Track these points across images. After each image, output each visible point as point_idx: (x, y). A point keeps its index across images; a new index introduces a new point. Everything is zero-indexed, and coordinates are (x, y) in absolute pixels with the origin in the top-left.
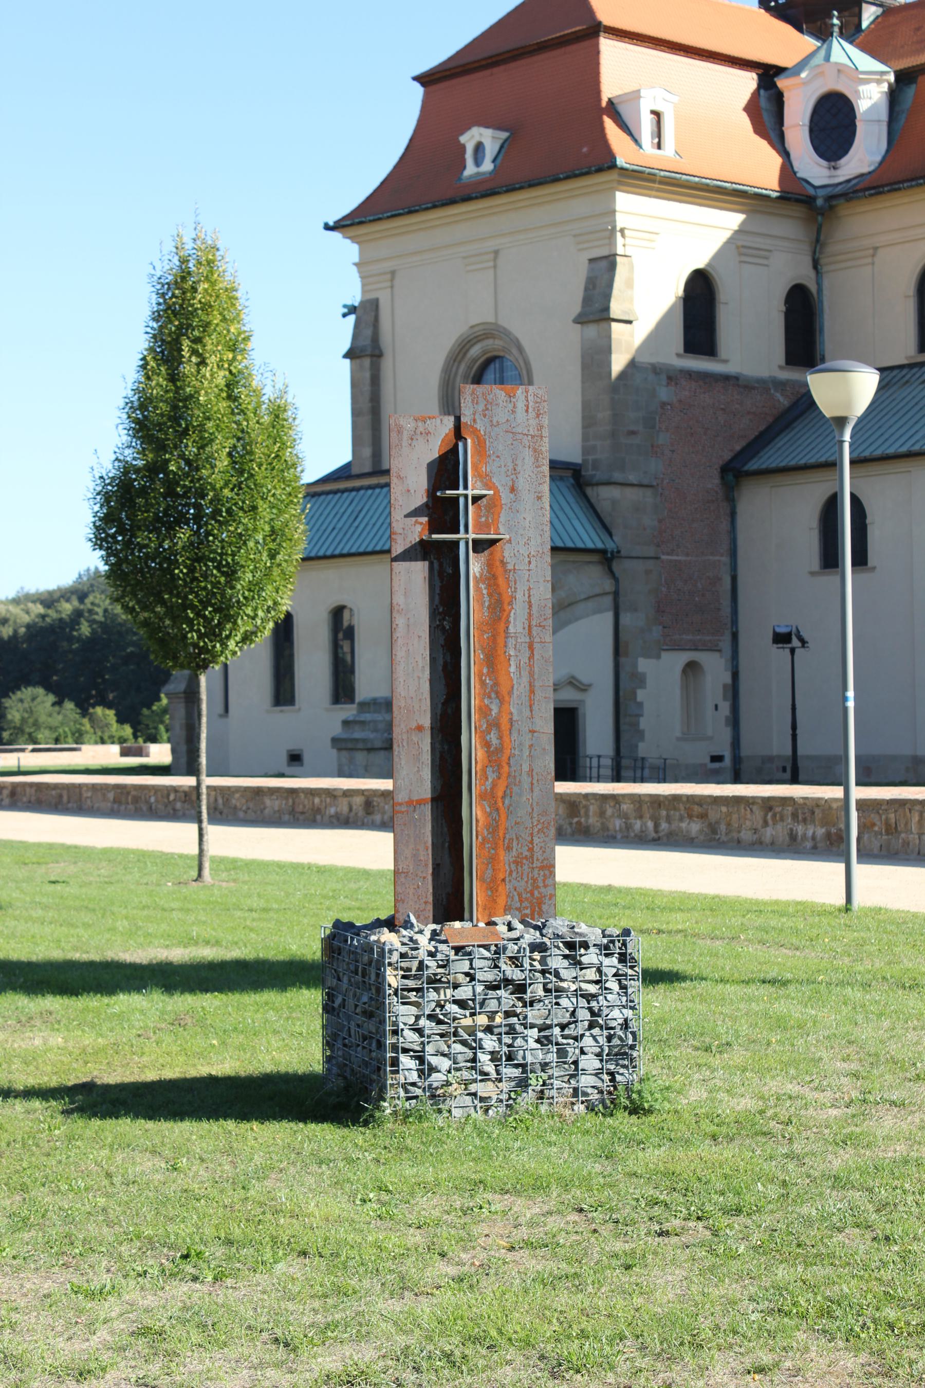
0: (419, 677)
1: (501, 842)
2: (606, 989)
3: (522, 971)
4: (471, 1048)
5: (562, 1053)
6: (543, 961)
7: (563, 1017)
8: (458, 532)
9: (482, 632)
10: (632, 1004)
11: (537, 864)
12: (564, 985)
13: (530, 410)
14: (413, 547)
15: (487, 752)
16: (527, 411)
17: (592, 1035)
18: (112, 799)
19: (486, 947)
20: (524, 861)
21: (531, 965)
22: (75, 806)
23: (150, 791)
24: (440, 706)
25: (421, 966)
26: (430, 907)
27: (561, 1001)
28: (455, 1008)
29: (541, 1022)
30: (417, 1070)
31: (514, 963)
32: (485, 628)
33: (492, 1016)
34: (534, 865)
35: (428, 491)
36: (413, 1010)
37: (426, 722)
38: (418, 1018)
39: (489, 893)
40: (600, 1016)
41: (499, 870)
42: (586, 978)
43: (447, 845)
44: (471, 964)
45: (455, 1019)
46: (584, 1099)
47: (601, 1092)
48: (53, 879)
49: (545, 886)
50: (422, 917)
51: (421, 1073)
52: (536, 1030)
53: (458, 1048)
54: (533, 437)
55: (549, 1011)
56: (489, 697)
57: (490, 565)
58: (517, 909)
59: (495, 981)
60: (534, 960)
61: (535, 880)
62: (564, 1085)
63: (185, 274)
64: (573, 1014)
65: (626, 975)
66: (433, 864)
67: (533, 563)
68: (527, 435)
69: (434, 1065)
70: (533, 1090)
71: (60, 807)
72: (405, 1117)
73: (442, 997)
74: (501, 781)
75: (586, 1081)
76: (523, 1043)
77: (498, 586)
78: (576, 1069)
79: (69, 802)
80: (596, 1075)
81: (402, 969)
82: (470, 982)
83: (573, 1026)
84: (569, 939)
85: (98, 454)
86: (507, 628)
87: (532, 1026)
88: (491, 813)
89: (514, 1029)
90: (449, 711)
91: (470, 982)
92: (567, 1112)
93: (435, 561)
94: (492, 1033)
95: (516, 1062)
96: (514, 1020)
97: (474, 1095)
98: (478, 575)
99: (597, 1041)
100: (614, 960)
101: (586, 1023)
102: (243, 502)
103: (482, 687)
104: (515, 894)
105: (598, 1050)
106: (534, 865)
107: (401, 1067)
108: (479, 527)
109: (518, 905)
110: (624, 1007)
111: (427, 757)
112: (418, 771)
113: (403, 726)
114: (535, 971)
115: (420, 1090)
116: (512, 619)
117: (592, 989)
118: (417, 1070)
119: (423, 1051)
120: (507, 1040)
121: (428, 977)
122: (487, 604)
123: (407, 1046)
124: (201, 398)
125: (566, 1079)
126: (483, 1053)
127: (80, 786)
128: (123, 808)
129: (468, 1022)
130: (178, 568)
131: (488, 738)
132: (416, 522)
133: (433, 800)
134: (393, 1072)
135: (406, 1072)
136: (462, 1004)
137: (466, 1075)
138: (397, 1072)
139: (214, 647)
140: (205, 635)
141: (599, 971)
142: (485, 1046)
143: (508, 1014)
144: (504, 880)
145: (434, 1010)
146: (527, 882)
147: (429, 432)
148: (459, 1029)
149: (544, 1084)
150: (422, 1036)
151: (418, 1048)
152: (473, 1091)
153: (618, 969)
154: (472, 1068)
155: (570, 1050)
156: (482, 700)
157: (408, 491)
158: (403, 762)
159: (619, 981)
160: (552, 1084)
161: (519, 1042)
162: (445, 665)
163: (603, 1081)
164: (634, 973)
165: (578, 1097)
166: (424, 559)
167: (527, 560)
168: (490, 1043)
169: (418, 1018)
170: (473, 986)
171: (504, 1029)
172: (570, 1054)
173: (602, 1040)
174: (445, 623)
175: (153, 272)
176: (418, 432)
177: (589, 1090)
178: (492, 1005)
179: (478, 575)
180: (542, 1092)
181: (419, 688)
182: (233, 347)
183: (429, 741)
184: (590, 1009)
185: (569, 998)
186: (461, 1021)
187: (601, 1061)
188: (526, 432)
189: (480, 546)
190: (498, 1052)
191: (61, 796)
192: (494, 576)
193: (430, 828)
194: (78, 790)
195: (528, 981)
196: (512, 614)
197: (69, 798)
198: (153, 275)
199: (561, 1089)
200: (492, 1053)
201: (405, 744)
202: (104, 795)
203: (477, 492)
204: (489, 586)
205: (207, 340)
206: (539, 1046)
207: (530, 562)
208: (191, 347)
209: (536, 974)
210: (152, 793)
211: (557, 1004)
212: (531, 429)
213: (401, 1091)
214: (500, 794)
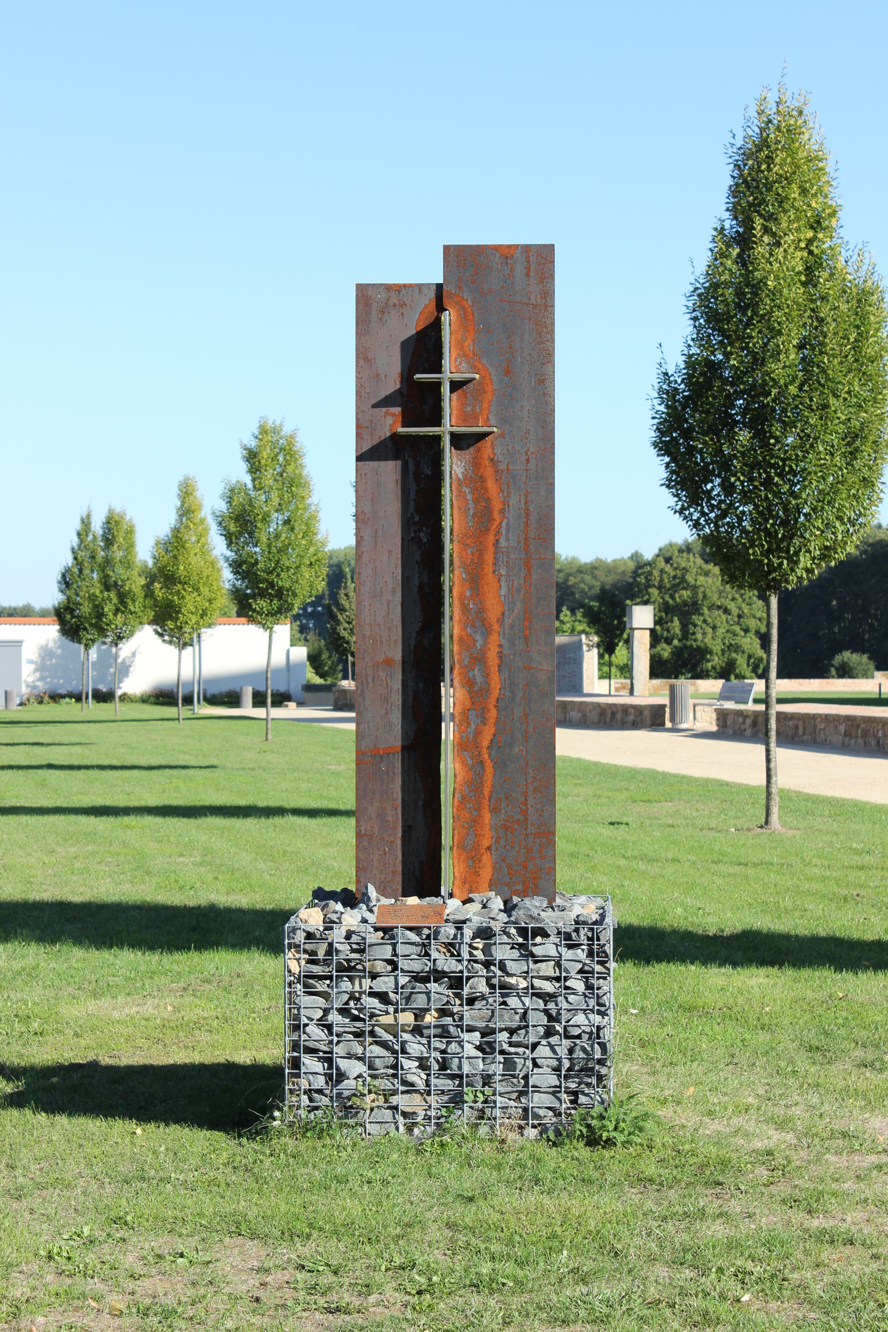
0: (388, 602)
1: (486, 802)
2: (567, 988)
3: (459, 961)
4: (395, 1052)
5: (509, 1064)
6: (486, 950)
7: (512, 1020)
8: (439, 424)
9: (464, 546)
10: (603, 1009)
11: (532, 830)
12: (512, 980)
13: (532, 273)
14: (383, 444)
15: (469, 692)
16: (528, 275)
17: (549, 1044)
18: (843, 732)
19: (416, 930)
20: (516, 826)
21: (471, 954)
22: (810, 738)
23: (878, 724)
24: (414, 635)
25: (330, 950)
26: (399, 878)
27: (509, 1000)
28: (374, 1002)
29: (484, 1024)
30: (325, 1074)
31: (449, 951)
32: (468, 542)
33: (419, 1014)
34: (529, 831)
35: (402, 374)
36: (320, 1001)
37: (397, 655)
38: (326, 1012)
39: (471, 863)
40: (559, 1021)
41: (484, 835)
42: (541, 974)
43: (421, 803)
44: (394, 950)
45: (372, 1016)
46: (536, 1122)
47: (558, 1114)
48: (613, 820)
49: (542, 857)
50: (389, 890)
51: (329, 1077)
52: (477, 1034)
53: (377, 1050)
54: (535, 306)
55: (493, 1011)
56: (473, 626)
57: (476, 464)
58: (505, 884)
59: (422, 972)
60: (476, 949)
61: (529, 850)
62: (512, 1103)
63: (763, 143)
64: (524, 1016)
65: (592, 972)
66: (403, 826)
67: (533, 463)
68: (528, 304)
69: (343, 1069)
70: (471, 1107)
71: (796, 739)
72: (305, 1129)
73: (357, 988)
74: (486, 728)
75: (539, 1101)
76: (459, 1050)
77: (486, 489)
78: (526, 1085)
79: (804, 734)
80: (554, 1093)
81: (305, 951)
82: (393, 971)
83: (523, 1031)
84: (523, 925)
85: (663, 349)
86: (497, 541)
87: (471, 1029)
88: (473, 766)
89: (449, 1032)
90: (426, 642)
91: (393, 971)
92: (512, 1136)
93: (410, 460)
94: (422, 1036)
95: (449, 1071)
96: (448, 1020)
97: (395, 1108)
98: (460, 476)
99: (554, 1051)
100: (581, 954)
101: (541, 1031)
102: (811, 400)
103: (463, 613)
104: (504, 865)
105: (555, 1063)
106: (529, 831)
107: (303, 1070)
108: (465, 418)
109: (507, 879)
110: (592, 1011)
111: (397, 699)
112: (387, 713)
113: (367, 659)
114: (476, 961)
115: (327, 1099)
116: (503, 531)
117: (548, 987)
118: (325, 1074)
119: (331, 1052)
120: (437, 1043)
121: (339, 964)
122: (471, 512)
123: (311, 1045)
124: (769, 283)
125: (514, 1096)
126: (409, 1058)
127: (814, 717)
128: (853, 742)
129: (388, 1020)
130: (735, 475)
131: (471, 675)
132: (387, 413)
133: (404, 748)
134: (292, 1075)
135: (310, 1077)
136: (383, 997)
137: (385, 1084)
138: (298, 1076)
139: (781, 564)
140: (770, 551)
141: (558, 964)
142: (409, 1050)
143: (443, 1012)
144: (488, 848)
145: (347, 1003)
146: (518, 852)
147: (405, 304)
148: (376, 1028)
149: (486, 1101)
150: (331, 1033)
151: (326, 1049)
152: (395, 1104)
153: (584, 964)
154: (395, 1076)
155: (519, 1061)
156: (464, 629)
157: (378, 375)
158: (367, 703)
159: (587, 978)
160: (495, 1102)
161: (453, 1047)
162: (421, 586)
163: (560, 1100)
164: (604, 970)
165: (527, 1119)
166: (396, 459)
167: (524, 457)
168: (415, 1047)
169: (326, 1012)
170: (396, 977)
171: (433, 1031)
172: (519, 1067)
173: (562, 1052)
174: (422, 535)
175: (733, 141)
176: (391, 303)
177: (542, 1112)
178: (420, 1001)
179: (460, 476)
180: (482, 1111)
181: (388, 614)
182: (817, 224)
183: (400, 677)
184: (546, 1012)
185: (520, 997)
186: (380, 1018)
187: (559, 1076)
188: (526, 300)
189: (460, 441)
190: (427, 1058)
191: (797, 727)
192: (481, 477)
193: (400, 783)
194: (812, 721)
195: (466, 974)
196: (504, 524)
197: (804, 729)
198: (732, 145)
199: (507, 1108)
200: (420, 1059)
201: (370, 680)
202: (836, 727)
203: (458, 377)
204: (474, 490)
205: (783, 218)
206: (480, 1054)
207: (528, 461)
208: (763, 224)
209: (475, 965)
210: (880, 727)
211: (504, 1003)
212: (533, 298)
213: (305, 1098)
214: (485, 743)
